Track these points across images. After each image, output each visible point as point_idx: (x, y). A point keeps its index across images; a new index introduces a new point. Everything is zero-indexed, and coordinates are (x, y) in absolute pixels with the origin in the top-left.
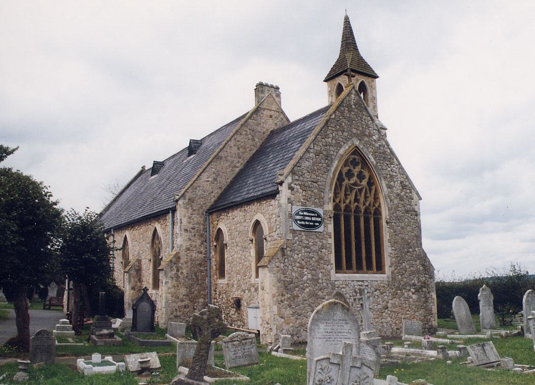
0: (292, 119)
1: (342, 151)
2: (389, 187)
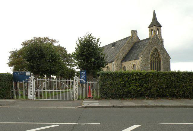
0: (141, 39)
1: (153, 49)
2: (163, 56)
